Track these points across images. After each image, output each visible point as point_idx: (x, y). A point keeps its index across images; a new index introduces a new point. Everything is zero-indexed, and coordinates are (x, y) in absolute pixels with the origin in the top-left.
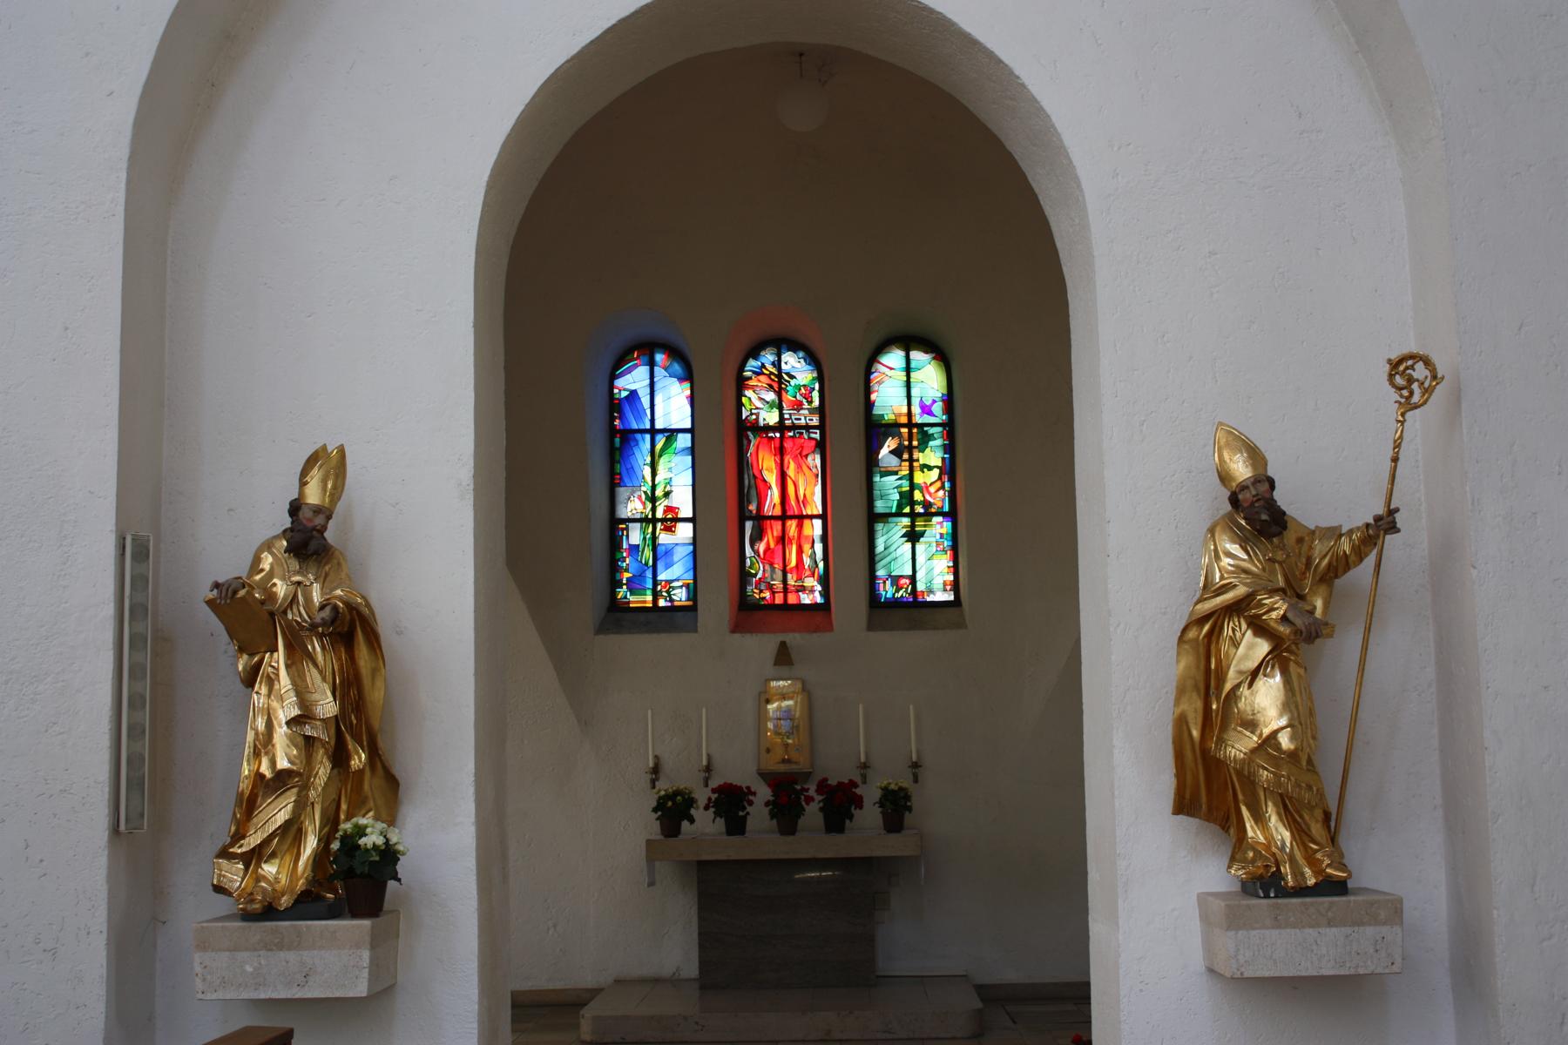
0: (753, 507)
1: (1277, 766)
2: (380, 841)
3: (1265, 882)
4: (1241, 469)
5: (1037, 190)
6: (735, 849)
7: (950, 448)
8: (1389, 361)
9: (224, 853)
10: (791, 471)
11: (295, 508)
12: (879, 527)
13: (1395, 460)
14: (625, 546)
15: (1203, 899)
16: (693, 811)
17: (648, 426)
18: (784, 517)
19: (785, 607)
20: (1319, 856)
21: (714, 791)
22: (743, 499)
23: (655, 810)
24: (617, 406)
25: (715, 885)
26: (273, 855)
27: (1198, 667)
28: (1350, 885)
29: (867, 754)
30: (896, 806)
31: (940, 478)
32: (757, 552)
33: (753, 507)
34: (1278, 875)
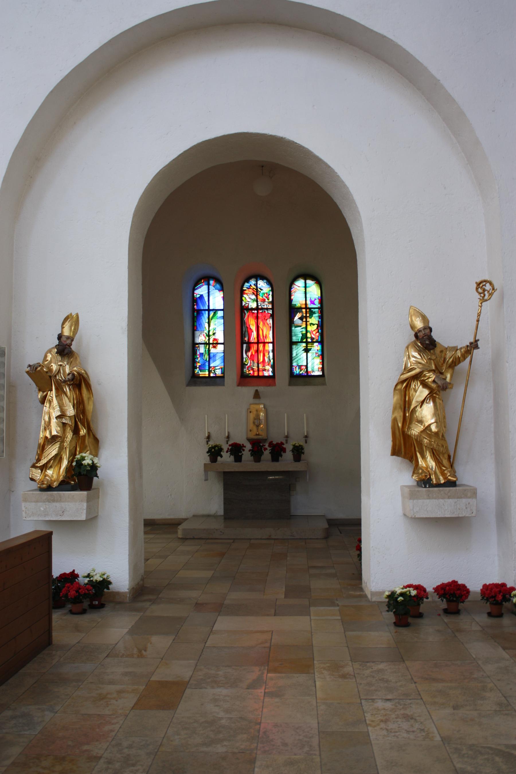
0: (246, 339)
1: (430, 438)
2: (90, 462)
3: (425, 482)
4: (419, 324)
5: (345, 217)
6: (237, 467)
7: (321, 317)
8: (476, 283)
9: (34, 466)
10: (261, 325)
11: (60, 337)
12: (294, 347)
13: (478, 321)
14: (198, 353)
15: (402, 487)
16: (222, 453)
17: (207, 308)
18: (258, 343)
19: (258, 377)
20: (446, 472)
21: (230, 445)
22: (242, 336)
23: (208, 452)
24: (195, 301)
25: (231, 481)
26: (51, 467)
27: (401, 400)
28: (457, 483)
29: (288, 432)
30: (298, 452)
31: (317, 328)
32: (248, 356)
33: (246, 339)
34: (430, 479)
